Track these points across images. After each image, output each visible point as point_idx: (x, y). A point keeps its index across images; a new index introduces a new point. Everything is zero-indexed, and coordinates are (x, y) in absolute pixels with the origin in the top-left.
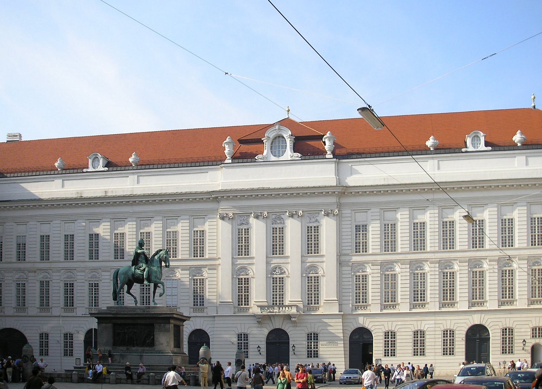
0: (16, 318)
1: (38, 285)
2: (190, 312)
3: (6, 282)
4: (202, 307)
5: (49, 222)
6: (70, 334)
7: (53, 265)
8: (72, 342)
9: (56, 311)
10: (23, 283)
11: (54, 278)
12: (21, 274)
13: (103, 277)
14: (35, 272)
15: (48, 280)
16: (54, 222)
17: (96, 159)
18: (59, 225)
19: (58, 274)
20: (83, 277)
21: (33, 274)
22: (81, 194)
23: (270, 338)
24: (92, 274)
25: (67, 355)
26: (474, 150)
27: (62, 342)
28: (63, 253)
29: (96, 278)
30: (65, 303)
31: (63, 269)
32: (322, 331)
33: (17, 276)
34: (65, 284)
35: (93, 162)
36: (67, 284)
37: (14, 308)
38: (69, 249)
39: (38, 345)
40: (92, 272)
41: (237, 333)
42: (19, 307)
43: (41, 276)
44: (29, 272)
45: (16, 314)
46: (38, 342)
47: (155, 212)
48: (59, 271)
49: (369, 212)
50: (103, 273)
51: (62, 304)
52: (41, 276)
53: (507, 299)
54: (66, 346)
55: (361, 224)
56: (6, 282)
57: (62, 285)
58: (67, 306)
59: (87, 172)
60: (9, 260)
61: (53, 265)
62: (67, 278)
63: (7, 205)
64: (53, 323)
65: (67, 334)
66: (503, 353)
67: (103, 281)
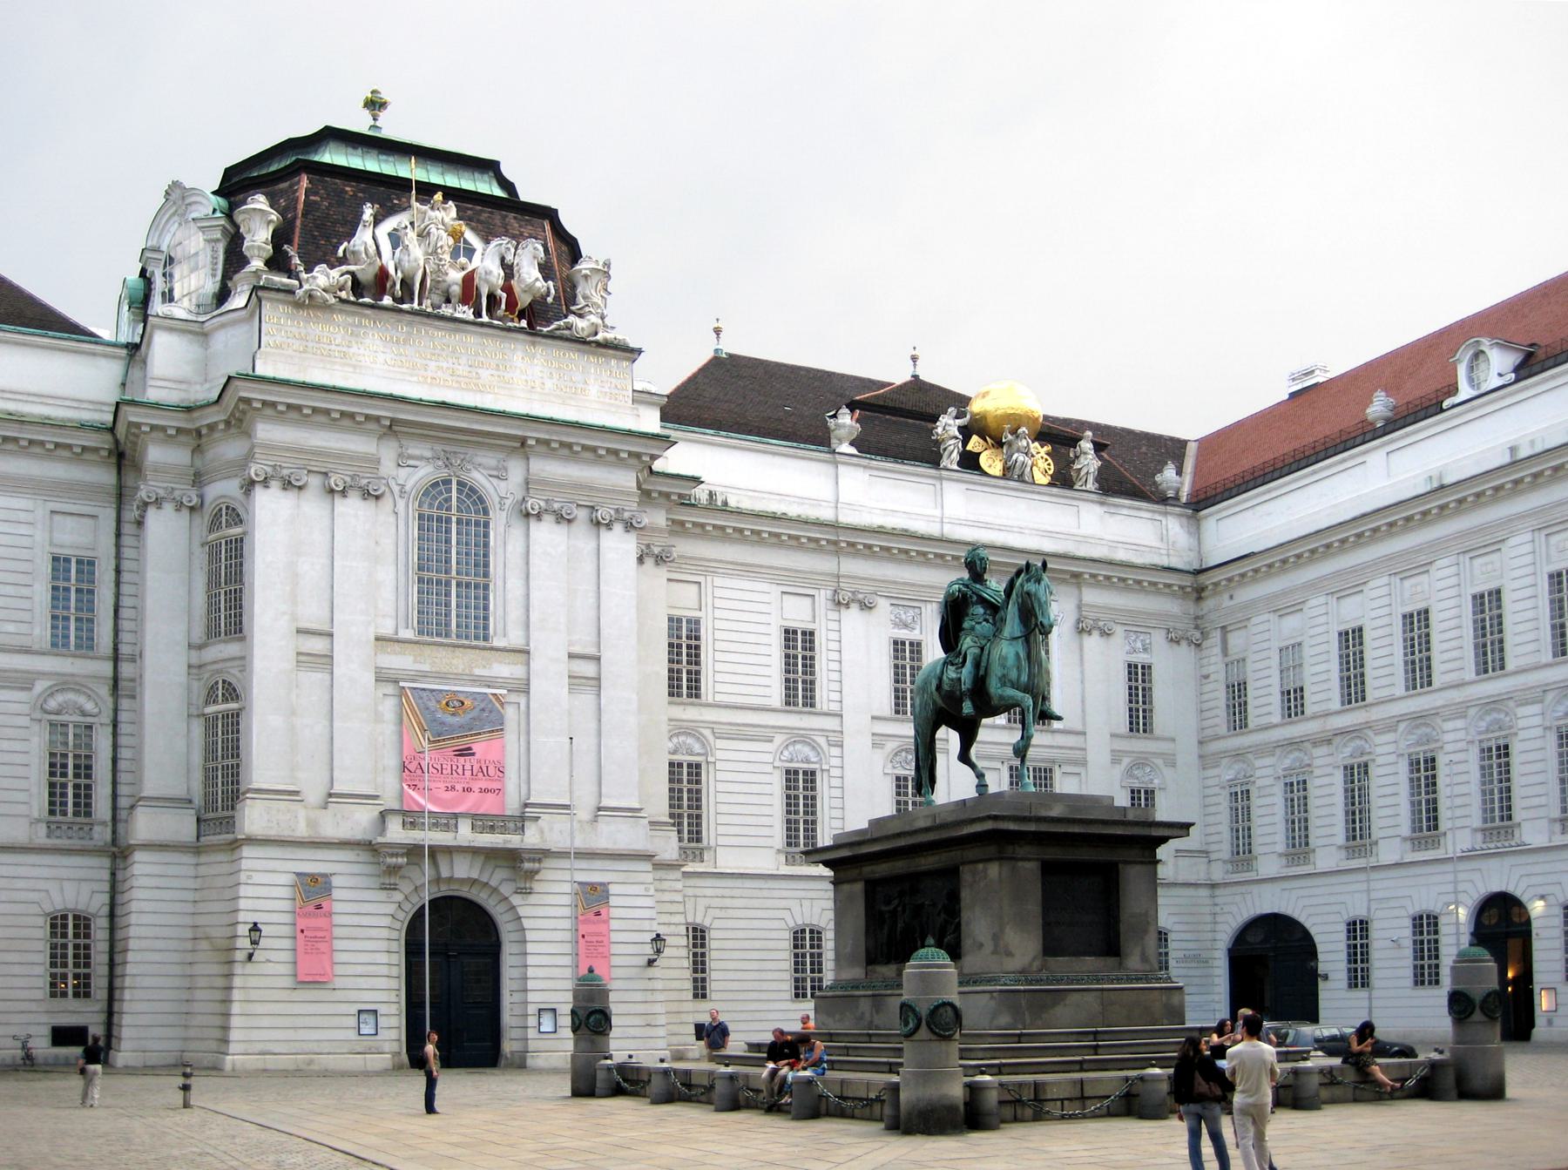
0: (1286, 885)
1: (1339, 778)
2: (1552, 833)
3: (1259, 783)
4: (1506, 823)
5: (1296, 608)
6: (1428, 917)
7: (1376, 714)
8: (1436, 941)
9: (1388, 852)
10: (1301, 778)
11: (1379, 750)
12: (1297, 754)
13: (1521, 723)
14: (1329, 742)
15: (1365, 758)
16: (1371, 584)
17: (1481, 358)
18: (1322, 610)
19: (1390, 737)
20: (1461, 735)
21: (1323, 750)
22: (1440, 477)
23: (1250, 939)
24: (1488, 718)
25: (1423, 983)
26: (1475, 393)
27: (1408, 943)
28: (1335, 683)
29: (1500, 729)
30: (1413, 821)
31: (1401, 719)
32: (717, 924)
33: (1287, 762)
34: (1483, 751)
35: (1471, 369)
36: (1490, 750)
37: (1280, 855)
38: (1417, 656)
39: (1344, 956)
40: (1417, 727)
41: (792, 924)
42: (1351, 843)
43: (1348, 751)
44: (1315, 744)
45: (1410, 857)
46: (1343, 946)
47: (1510, 520)
48: (1392, 728)
49: (1433, 568)
50: (1521, 711)
51: (1340, 839)
52: (1345, 753)
53: (1498, 823)
54: (1419, 954)
55: (1349, 626)
56: (1259, 783)
57: (1403, 768)
58: (1421, 830)
59: (1454, 406)
60: (1264, 721)
61: (1376, 714)
62: (1418, 743)
63: (1246, 567)
64: (1383, 885)
65: (1421, 918)
66: (797, 995)
67: (1522, 735)
